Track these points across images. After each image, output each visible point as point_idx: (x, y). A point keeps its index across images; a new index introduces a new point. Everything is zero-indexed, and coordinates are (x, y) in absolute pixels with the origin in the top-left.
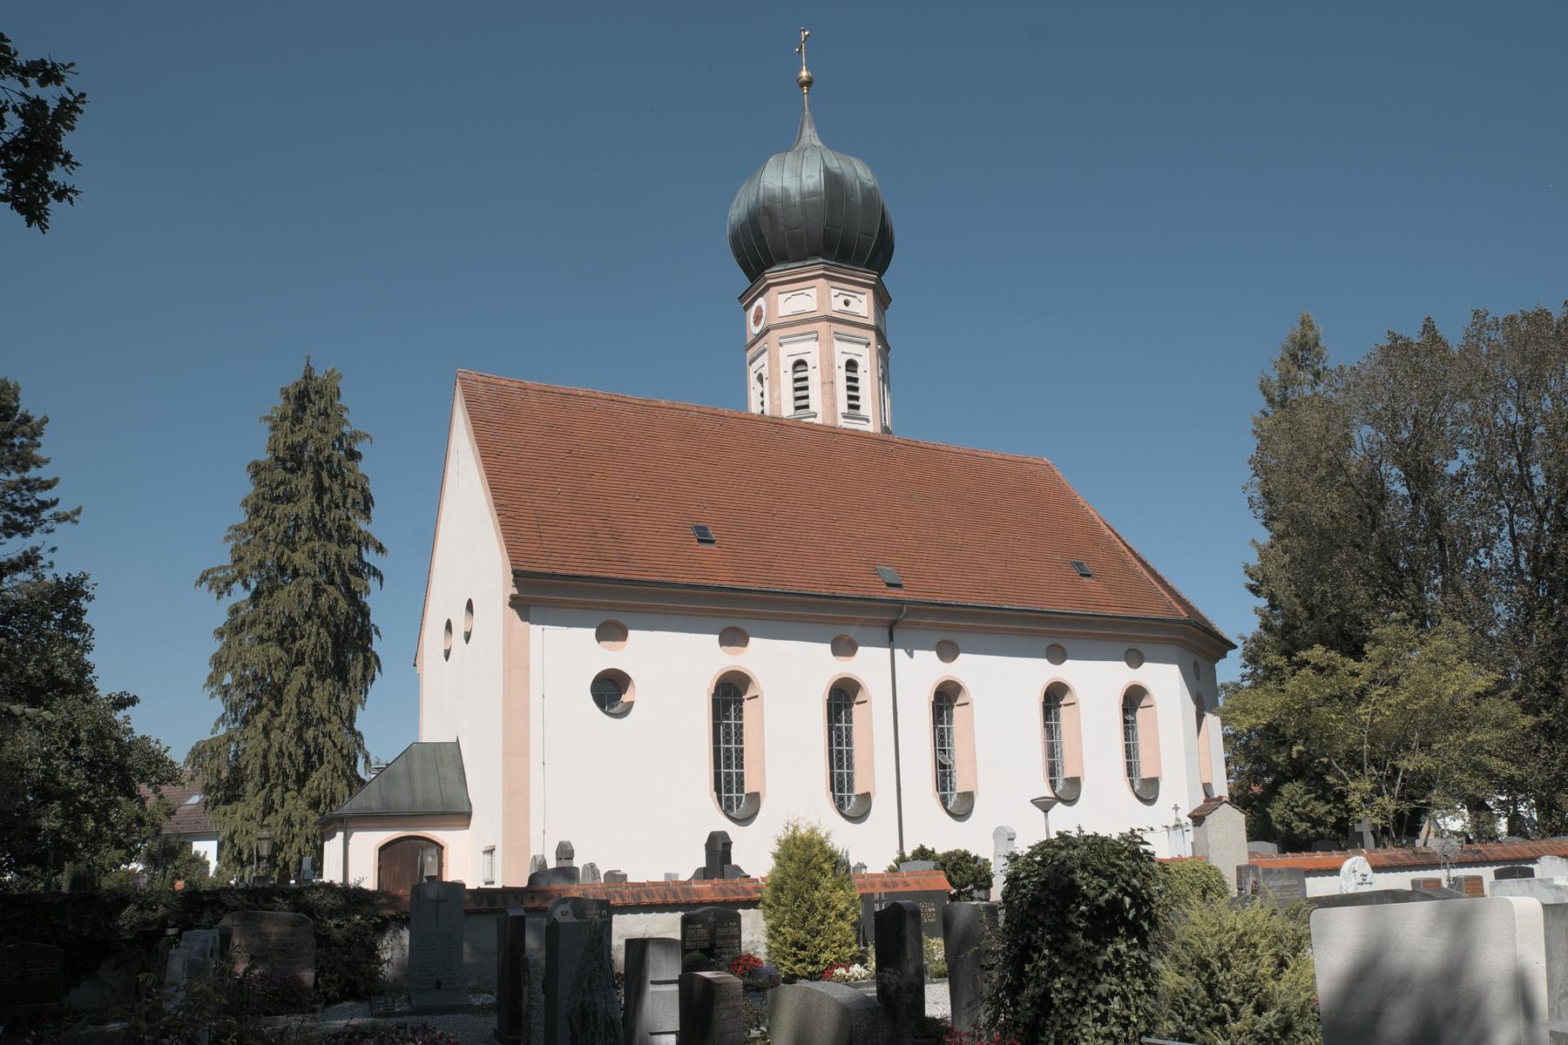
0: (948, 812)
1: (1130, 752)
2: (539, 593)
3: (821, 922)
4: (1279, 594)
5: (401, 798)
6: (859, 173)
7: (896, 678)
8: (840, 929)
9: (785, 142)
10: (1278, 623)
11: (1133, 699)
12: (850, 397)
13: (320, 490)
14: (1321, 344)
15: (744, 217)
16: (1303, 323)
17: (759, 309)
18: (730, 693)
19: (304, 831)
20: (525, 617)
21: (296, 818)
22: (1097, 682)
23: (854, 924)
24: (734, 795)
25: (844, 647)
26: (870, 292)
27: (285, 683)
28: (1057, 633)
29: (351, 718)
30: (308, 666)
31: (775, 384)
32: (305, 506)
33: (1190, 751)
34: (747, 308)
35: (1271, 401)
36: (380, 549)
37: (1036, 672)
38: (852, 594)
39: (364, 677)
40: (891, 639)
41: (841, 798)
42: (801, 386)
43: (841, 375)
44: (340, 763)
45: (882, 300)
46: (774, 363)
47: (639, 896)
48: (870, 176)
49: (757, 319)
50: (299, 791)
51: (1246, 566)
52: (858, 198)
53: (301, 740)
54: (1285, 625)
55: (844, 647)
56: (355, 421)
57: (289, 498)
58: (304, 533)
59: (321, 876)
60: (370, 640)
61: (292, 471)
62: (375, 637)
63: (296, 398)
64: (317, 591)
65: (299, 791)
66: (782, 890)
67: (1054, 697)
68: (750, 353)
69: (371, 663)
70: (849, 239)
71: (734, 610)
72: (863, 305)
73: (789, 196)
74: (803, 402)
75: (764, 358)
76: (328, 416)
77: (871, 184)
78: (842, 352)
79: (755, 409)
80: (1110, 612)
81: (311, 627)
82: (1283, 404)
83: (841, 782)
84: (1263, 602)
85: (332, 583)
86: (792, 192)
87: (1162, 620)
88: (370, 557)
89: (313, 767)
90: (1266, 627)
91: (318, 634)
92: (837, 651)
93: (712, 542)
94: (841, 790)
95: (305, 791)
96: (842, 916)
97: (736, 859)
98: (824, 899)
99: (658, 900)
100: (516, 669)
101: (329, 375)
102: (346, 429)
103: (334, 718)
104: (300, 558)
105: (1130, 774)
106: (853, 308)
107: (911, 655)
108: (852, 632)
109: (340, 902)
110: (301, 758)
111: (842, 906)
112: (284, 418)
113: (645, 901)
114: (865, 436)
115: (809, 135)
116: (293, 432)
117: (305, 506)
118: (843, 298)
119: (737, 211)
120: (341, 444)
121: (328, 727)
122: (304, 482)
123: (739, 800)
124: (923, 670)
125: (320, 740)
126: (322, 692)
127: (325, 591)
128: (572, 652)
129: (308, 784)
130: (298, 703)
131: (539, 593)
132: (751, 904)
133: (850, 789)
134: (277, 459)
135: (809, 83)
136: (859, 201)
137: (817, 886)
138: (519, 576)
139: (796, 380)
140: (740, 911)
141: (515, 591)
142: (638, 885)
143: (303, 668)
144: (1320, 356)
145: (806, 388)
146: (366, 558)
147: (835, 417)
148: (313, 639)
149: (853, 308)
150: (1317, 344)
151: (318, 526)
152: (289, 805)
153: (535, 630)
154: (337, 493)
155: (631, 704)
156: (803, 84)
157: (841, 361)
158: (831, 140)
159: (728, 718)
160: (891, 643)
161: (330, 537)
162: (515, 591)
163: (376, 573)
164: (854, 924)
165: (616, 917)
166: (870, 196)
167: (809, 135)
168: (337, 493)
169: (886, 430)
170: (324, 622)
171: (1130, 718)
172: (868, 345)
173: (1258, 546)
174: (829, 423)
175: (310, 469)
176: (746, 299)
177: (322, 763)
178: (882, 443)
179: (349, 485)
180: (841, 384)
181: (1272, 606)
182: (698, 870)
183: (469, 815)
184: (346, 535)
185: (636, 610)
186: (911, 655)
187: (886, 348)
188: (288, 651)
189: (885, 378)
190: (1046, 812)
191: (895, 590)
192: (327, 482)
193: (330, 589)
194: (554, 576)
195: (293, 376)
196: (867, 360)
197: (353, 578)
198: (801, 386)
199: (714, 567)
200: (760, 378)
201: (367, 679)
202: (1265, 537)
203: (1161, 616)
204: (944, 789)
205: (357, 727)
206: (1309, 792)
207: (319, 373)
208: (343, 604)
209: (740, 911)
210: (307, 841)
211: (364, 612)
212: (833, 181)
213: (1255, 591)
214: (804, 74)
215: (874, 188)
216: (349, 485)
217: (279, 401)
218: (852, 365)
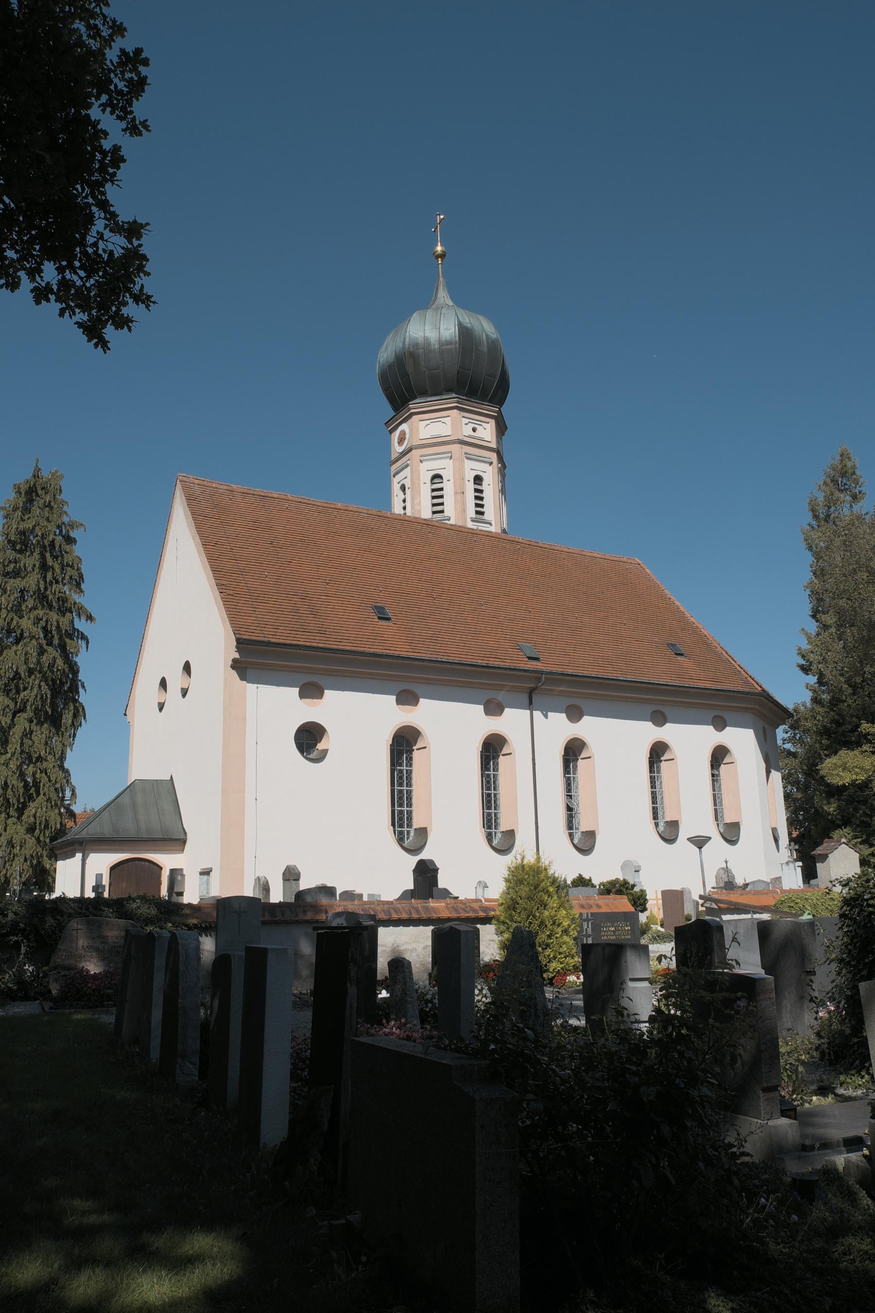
0: (573, 844)
1: (716, 800)
2: (257, 658)
3: (549, 937)
4: (827, 672)
5: (129, 828)
6: (485, 328)
7: (536, 734)
8: (565, 943)
9: (424, 302)
10: (825, 697)
11: (719, 756)
12: (477, 505)
13: (44, 567)
14: (858, 472)
15: (392, 359)
16: (842, 455)
17: (403, 433)
18: (404, 743)
19: (23, 852)
20: (243, 677)
21: (17, 840)
22: (690, 741)
23: (575, 939)
24: (406, 829)
25: (494, 709)
26: (493, 422)
27: (10, 728)
28: (659, 700)
29: (62, 758)
30: (29, 713)
31: (416, 492)
32: (32, 581)
33: (760, 797)
34: (391, 432)
35: (816, 517)
36: (90, 618)
37: (645, 733)
38: (501, 664)
39: (73, 724)
40: (531, 703)
41: (401, 833)
42: (437, 495)
43: (470, 487)
44: (54, 796)
45: (501, 428)
46: (415, 476)
47: (390, 914)
48: (493, 330)
49: (401, 441)
50: (19, 818)
51: (800, 649)
52: (485, 348)
53: (22, 776)
54: (833, 698)
55: (494, 709)
56: (73, 512)
57: (16, 574)
58: (30, 603)
59: (51, 889)
60: (78, 693)
61: (20, 552)
62: (81, 690)
63: (27, 493)
64: (42, 652)
65: (19, 818)
66: (514, 909)
67: (658, 752)
68: (394, 468)
69: (79, 713)
70: (475, 379)
71: (408, 675)
72: (487, 432)
73: (430, 344)
74: (439, 508)
75: (407, 472)
76: (51, 508)
77: (494, 336)
78: (471, 468)
79: (397, 509)
80: (702, 685)
81: (35, 681)
82: (827, 518)
83: (401, 819)
84: (812, 679)
85: (50, 644)
86: (432, 341)
87: (743, 693)
88: (81, 624)
89: (31, 798)
90: (816, 700)
91: (40, 687)
92: (488, 712)
93: (389, 619)
94: (401, 826)
95: (24, 817)
96: (566, 932)
97: (443, 881)
98: (552, 917)
99: (405, 916)
100: (234, 719)
101: (53, 475)
102: (65, 519)
103: (50, 757)
104: (26, 623)
105: (717, 819)
107: (546, 716)
108: (500, 696)
109: (154, 911)
110: (21, 791)
111: (565, 924)
112: (15, 509)
113: (395, 916)
114: (489, 535)
115: (443, 296)
116: (23, 520)
117: (32, 581)
118: (471, 426)
119: (386, 353)
120: (61, 531)
121: (45, 764)
122: (30, 561)
123: (408, 833)
124: (556, 728)
125: (38, 776)
126: (41, 733)
127: (46, 651)
128: (279, 707)
129: (26, 813)
130: (22, 744)
131: (257, 658)
132: (486, 921)
133: (410, 825)
134: (9, 541)
135: (442, 256)
136: (485, 350)
137: (545, 906)
138: (242, 644)
139: (433, 490)
140: (478, 926)
141: (237, 656)
142: (388, 903)
143: (25, 715)
144: (856, 482)
145: (442, 497)
146: (77, 625)
147: (465, 520)
148: (34, 691)
150: (854, 473)
151: (42, 598)
152: (11, 830)
153: (251, 687)
154: (58, 571)
155: (325, 752)
156: (438, 257)
157: (470, 476)
158: (460, 300)
159: (401, 765)
160: (530, 705)
161: (51, 607)
162: (237, 656)
163: (84, 637)
164: (575, 939)
165: (382, 931)
166: (494, 347)
167: (443, 296)
168: (58, 571)
169: (504, 531)
170: (45, 678)
171: (716, 772)
172: (491, 463)
173: (807, 634)
174: (460, 524)
175: (38, 551)
176: (391, 425)
177: (38, 794)
178: (500, 540)
179: (68, 565)
180: (470, 494)
181: (820, 682)
182: (406, 892)
183: (184, 842)
184: (64, 607)
186: (546, 716)
187: (504, 466)
188: (14, 700)
189: (503, 491)
190: (700, 848)
191: (535, 663)
192: (50, 561)
193: (50, 649)
194: (269, 644)
195: (24, 476)
196: (490, 475)
197: (68, 641)
198: (437, 495)
199: (392, 640)
200: (403, 488)
201: (75, 725)
202: (812, 627)
203: (741, 689)
204: (489, 827)
205: (66, 765)
206: (856, 837)
207: (45, 474)
208: (60, 662)
209: (478, 926)
210: (26, 860)
211: (74, 669)
212: (465, 333)
213: (805, 669)
214: (439, 248)
215: (497, 340)
216: (68, 565)
217: (12, 495)
218: (478, 479)
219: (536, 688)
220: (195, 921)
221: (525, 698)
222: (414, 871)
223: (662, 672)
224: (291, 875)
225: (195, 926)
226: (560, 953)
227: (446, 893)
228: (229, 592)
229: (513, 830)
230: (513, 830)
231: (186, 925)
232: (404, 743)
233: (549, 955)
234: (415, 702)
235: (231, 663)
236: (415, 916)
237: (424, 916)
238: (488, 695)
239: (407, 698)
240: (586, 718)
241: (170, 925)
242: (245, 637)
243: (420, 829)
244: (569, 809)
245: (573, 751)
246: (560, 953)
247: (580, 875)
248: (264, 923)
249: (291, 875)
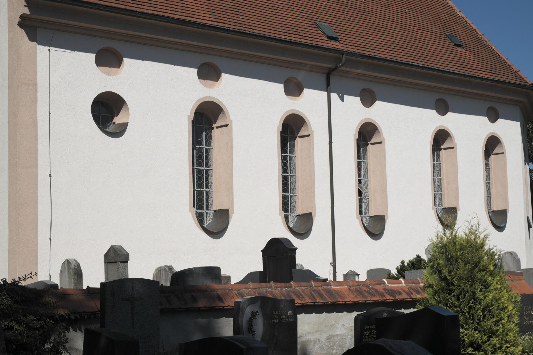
3: (496, 323)
7: (333, 115)
8: (510, 330)
11: (492, 145)
18: (206, 119)
20: (32, 38)
40: (328, 84)
55: (293, 89)
67: (441, 138)
71: (212, 47)
99: (308, 301)
100: (22, 88)
107: (342, 100)
108: (301, 76)
124: (351, 111)
137: (486, 286)
141: (27, 11)
153: (42, 50)
160: (328, 87)
162: (27, 11)
165: (301, 318)
191: (334, 43)
219: (336, 68)
220: (62, 312)
221: (322, 79)
222: (264, 252)
223: (445, 60)
224: (116, 257)
225: (62, 318)
226: (507, 342)
227: (309, 276)
229: (310, 214)
230: (310, 214)
231: (52, 318)
232: (206, 119)
233: (495, 345)
234: (216, 77)
235: (18, 19)
236: (319, 300)
237: (329, 300)
238: (289, 73)
240: (378, 103)
241: (32, 317)
244: (360, 193)
245: (367, 134)
246: (507, 342)
247: (418, 256)
248: (162, 311)
249: (116, 257)
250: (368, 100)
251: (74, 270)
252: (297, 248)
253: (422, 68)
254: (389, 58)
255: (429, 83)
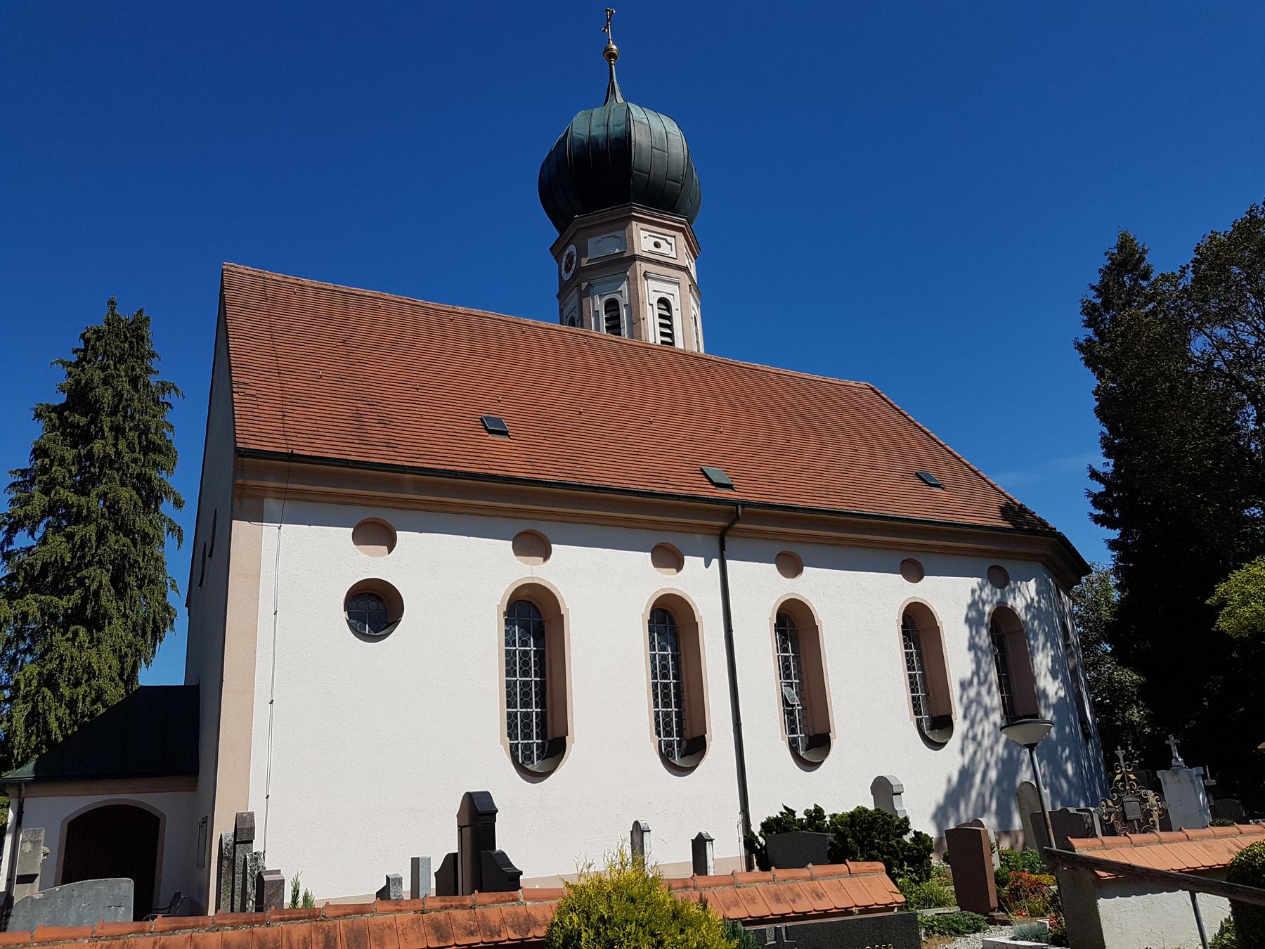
25: (669, 558)
40: (723, 548)
48: (679, 145)
71: (535, 509)
73: (597, 144)
86: (600, 141)
92: (658, 562)
93: (505, 433)
106: (665, 248)
124: (759, 586)
149: (665, 248)
185: (406, 505)
194: (291, 457)
221: (714, 543)
228: (248, 392)
239: (533, 545)
242: (252, 447)
243: (694, 739)
250: (791, 566)
251: (1113, 545)
252: (521, 873)
253: (868, 516)
254: (814, 506)
255: (935, 543)
